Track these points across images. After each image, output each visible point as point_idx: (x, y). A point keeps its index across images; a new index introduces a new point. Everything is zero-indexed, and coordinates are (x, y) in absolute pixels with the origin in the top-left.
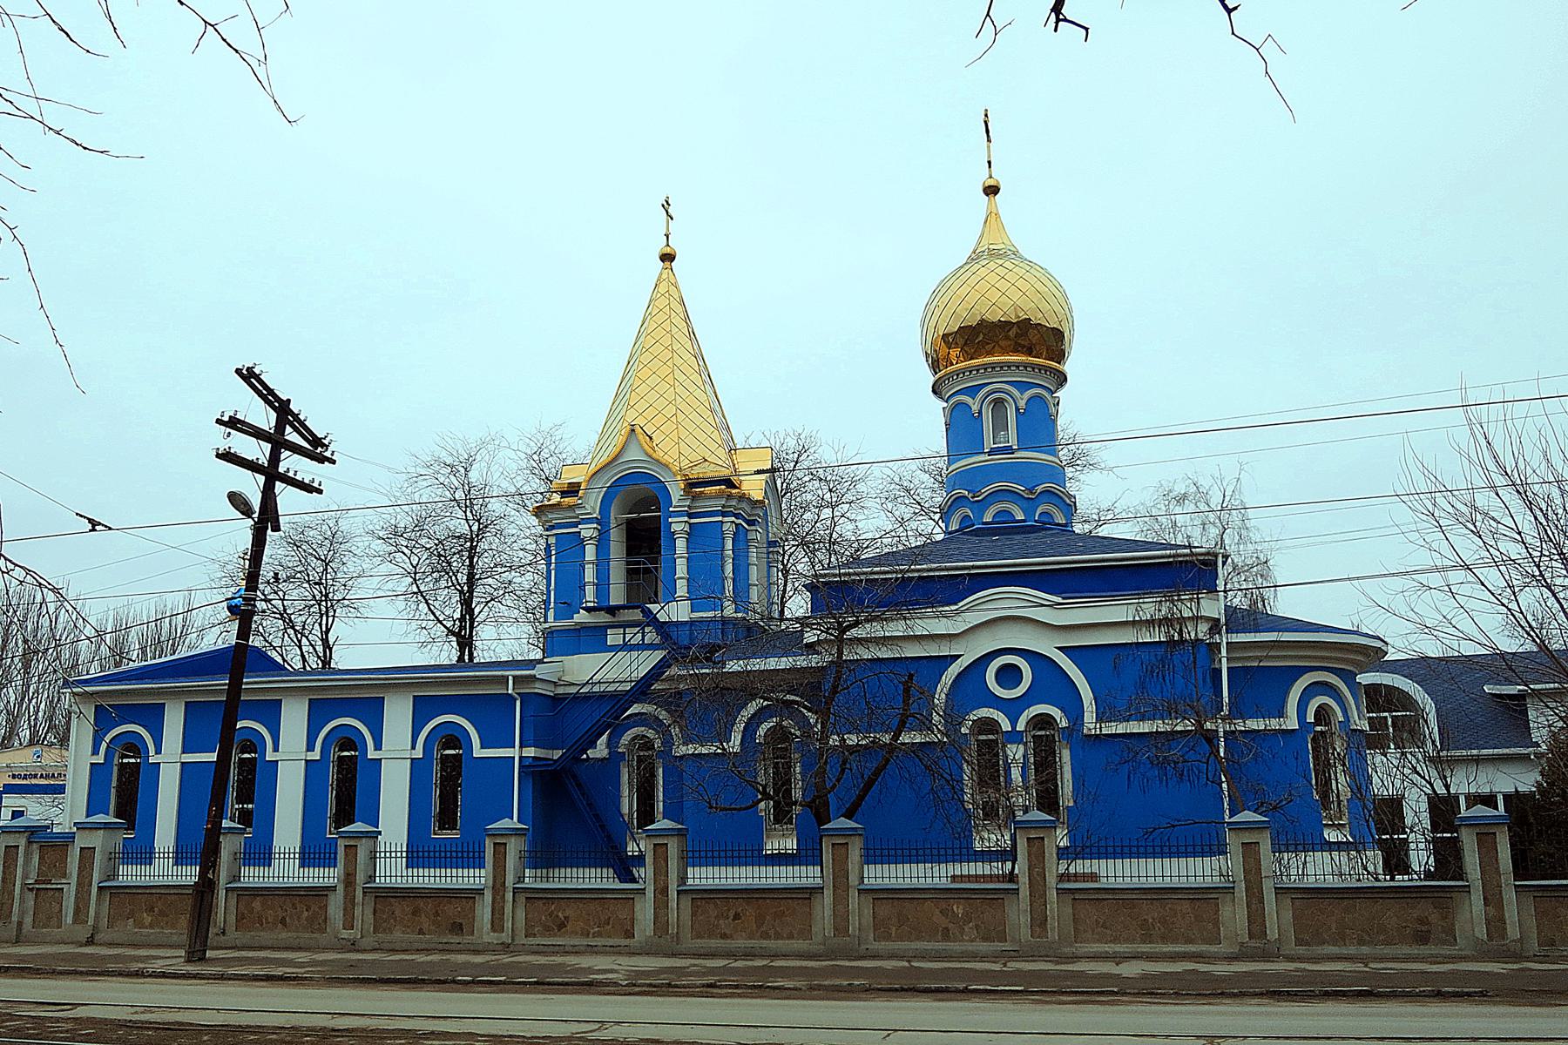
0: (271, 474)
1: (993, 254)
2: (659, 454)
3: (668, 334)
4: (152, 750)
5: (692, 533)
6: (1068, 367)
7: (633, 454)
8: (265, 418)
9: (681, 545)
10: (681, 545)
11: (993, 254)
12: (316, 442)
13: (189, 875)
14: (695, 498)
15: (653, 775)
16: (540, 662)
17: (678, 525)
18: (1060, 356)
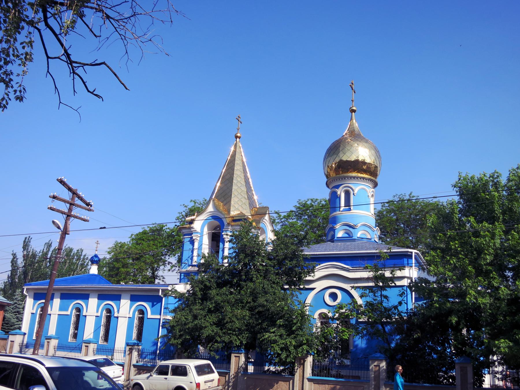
0: (69, 216)
4: (116, 310)
8: (67, 195)
12: (88, 204)
15: (342, 378)
16: (182, 254)
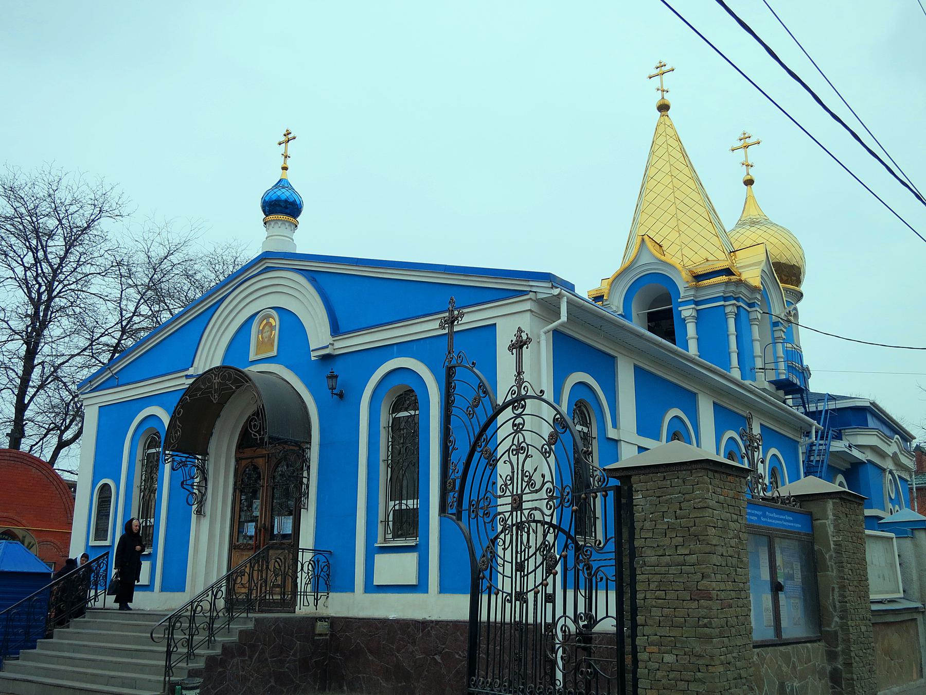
1: (753, 223)
2: (667, 258)
3: (669, 157)
5: (700, 317)
6: (803, 288)
7: (644, 259)
9: (691, 329)
10: (691, 329)
11: (753, 223)
13: (185, 650)
14: (697, 288)
17: (687, 312)
18: (798, 282)
